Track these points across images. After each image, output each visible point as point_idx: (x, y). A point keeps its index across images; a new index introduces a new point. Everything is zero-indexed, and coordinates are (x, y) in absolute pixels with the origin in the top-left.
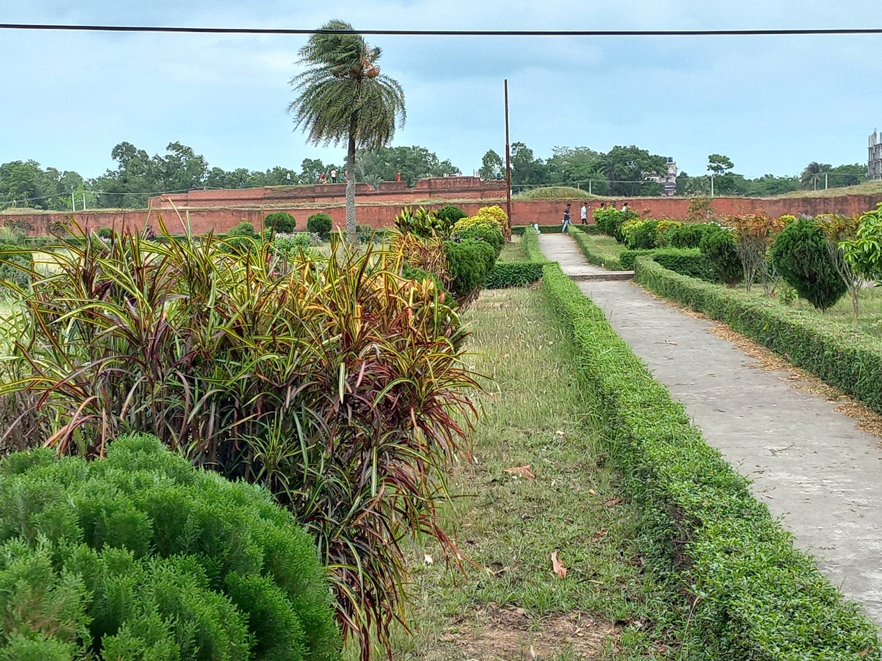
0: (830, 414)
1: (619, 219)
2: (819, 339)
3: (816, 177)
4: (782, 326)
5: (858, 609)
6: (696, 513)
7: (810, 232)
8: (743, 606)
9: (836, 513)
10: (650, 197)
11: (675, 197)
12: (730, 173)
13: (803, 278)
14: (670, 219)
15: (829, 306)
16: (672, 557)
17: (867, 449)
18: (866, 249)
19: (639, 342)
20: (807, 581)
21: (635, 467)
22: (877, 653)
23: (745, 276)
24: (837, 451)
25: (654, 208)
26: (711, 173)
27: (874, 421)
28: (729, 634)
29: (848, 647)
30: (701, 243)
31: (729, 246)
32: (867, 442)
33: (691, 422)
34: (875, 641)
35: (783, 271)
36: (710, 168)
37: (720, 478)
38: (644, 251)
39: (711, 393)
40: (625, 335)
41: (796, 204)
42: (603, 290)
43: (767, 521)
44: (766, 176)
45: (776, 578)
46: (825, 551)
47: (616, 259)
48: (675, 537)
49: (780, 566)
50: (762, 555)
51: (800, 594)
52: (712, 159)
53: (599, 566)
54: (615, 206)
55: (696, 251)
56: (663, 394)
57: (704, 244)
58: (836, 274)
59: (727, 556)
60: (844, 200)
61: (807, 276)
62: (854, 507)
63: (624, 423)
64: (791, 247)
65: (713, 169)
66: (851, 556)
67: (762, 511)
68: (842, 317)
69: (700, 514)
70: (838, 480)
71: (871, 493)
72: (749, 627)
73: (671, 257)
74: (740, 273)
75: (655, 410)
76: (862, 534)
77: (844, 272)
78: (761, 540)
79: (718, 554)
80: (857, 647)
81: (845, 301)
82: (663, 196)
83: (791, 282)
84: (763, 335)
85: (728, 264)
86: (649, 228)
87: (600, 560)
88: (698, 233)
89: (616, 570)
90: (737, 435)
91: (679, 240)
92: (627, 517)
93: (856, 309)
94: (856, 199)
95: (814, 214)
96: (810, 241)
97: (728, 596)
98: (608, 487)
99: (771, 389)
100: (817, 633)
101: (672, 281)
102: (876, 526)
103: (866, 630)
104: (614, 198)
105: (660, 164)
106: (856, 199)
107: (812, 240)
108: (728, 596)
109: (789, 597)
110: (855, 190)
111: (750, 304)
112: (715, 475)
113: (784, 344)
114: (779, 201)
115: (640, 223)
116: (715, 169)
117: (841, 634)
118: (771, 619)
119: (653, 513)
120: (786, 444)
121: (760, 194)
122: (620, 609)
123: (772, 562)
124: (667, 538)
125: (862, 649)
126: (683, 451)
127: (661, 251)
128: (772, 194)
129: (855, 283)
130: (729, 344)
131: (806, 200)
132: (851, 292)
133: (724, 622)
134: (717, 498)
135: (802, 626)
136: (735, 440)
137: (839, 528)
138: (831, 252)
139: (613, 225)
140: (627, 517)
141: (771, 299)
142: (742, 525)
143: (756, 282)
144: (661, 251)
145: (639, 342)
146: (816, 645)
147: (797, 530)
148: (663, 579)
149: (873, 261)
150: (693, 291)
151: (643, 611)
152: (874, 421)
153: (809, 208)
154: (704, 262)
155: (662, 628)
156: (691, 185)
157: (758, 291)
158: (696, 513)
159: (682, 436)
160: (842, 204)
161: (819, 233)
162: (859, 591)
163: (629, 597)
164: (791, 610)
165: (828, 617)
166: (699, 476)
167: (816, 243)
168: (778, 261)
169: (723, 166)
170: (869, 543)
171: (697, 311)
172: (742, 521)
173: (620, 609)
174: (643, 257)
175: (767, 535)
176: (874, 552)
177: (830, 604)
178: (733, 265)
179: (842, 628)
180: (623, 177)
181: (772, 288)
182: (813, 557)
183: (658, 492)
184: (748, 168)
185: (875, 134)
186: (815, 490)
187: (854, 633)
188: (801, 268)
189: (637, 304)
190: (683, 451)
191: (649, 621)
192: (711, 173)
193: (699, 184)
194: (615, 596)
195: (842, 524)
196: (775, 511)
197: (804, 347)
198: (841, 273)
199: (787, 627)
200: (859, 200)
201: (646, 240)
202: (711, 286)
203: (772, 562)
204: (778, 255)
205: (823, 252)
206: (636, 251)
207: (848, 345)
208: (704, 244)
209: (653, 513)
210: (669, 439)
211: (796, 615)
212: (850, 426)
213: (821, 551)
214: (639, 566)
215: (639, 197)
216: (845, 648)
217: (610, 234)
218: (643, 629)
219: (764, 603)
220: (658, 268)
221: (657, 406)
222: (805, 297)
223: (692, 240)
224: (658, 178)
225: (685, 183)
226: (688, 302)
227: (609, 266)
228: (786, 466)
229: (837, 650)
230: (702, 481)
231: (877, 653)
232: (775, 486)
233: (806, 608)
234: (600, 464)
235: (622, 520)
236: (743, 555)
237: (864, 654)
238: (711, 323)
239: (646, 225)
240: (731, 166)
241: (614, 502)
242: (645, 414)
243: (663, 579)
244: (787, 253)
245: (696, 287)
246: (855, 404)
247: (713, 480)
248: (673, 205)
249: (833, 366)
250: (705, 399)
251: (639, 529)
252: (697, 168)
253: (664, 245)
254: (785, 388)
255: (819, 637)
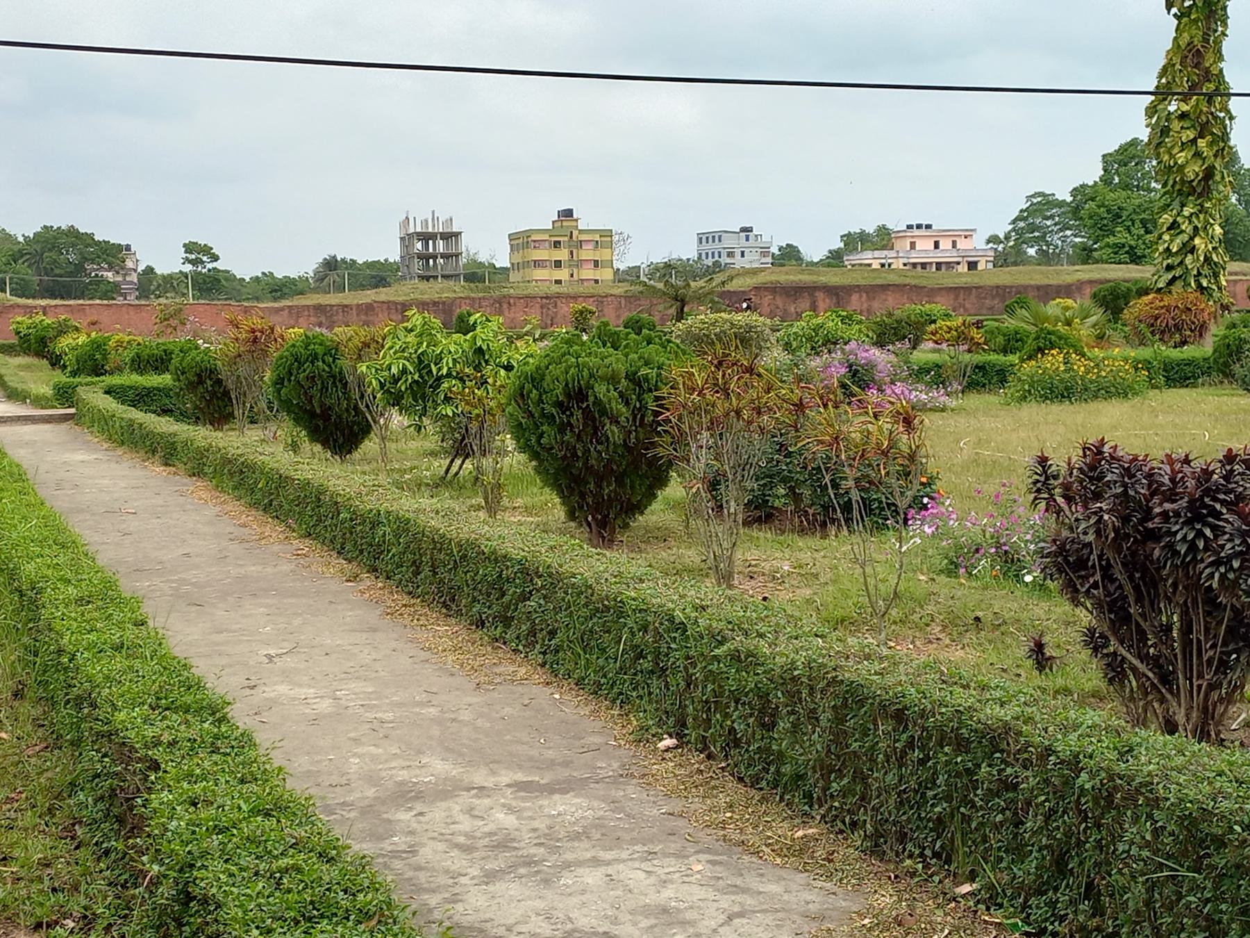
0: (348, 601)
1: (51, 334)
2: (332, 497)
3: (333, 277)
4: (283, 481)
5: (368, 863)
6: (150, 753)
7: (320, 350)
8: (212, 878)
9: (352, 735)
10: (98, 302)
11: (137, 302)
12: (214, 269)
13: (313, 414)
14: (129, 330)
15: (350, 452)
16: (120, 820)
17: (393, 644)
18: (394, 370)
19: (80, 511)
20: (301, 833)
21: (67, 694)
22: (391, 921)
23: (236, 412)
24: (356, 650)
25: (105, 317)
26: (188, 268)
27: (405, 606)
28: (192, 920)
29: (352, 917)
30: (171, 368)
31: (212, 372)
32: (395, 635)
33: (151, 623)
34: (389, 904)
35: (287, 406)
36: (187, 260)
37: (188, 699)
38: (89, 379)
39: (184, 580)
40: (59, 501)
41: (306, 313)
42: (27, 438)
43: (253, 754)
44: (263, 273)
45: (259, 832)
46: (336, 790)
47: (46, 390)
48: (122, 790)
49: (267, 815)
50: (241, 802)
51: (292, 851)
52: (190, 248)
53: (11, 846)
54: (43, 313)
55: (166, 379)
56: (109, 584)
57: (177, 368)
58: (356, 408)
59: (192, 809)
60: (369, 308)
61: (318, 411)
62: (376, 725)
63: (50, 630)
64: (295, 372)
65: (190, 262)
66: (371, 793)
67: (247, 741)
68: (367, 468)
69: (157, 754)
70: (357, 690)
71: (400, 705)
72: (219, 906)
73: (131, 387)
74: (229, 409)
75: (98, 609)
76: (386, 761)
77: (367, 406)
78: (242, 781)
79: (179, 808)
80: (365, 915)
81: (370, 446)
82: (120, 300)
83: (297, 421)
84: (259, 496)
85: (211, 397)
86: (98, 346)
87: (15, 835)
88: (168, 353)
89: (37, 848)
90: (222, 637)
91: (142, 364)
92: (56, 768)
93: (384, 453)
94: (385, 306)
95: (330, 328)
96: (320, 363)
97: (192, 866)
98: (30, 727)
99: (269, 570)
100: (312, 903)
101: (131, 423)
102: (403, 748)
103: (377, 890)
104: (43, 302)
105: (114, 254)
106: (385, 306)
107: (324, 362)
108: (192, 866)
109: (276, 857)
110: (383, 294)
111: (239, 452)
112: (183, 696)
113: (286, 507)
114: (282, 309)
115: (82, 339)
116: (194, 262)
117: (344, 901)
118: (249, 891)
119: (91, 759)
120: (287, 646)
121: (257, 299)
122: (41, 904)
123: (255, 812)
124: (113, 793)
125: (370, 918)
126: (137, 664)
127: (116, 380)
128: (275, 299)
129: (382, 421)
130: (211, 511)
131: (319, 309)
132: (378, 433)
133: (187, 904)
134: (183, 727)
135: (290, 896)
136: (218, 645)
137: (355, 755)
138: (350, 379)
139: (43, 341)
140: (56, 768)
141: (272, 445)
142: (216, 763)
143: (252, 422)
144: (116, 380)
145: (80, 511)
146: (310, 919)
147: (301, 763)
148: (107, 852)
149: (403, 388)
150: (161, 435)
151: (76, 904)
152: (405, 606)
153: (323, 319)
154: (178, 395)
155: (106, 923)
156: (159, 285)
157: (253, 434)
158: (150, 753)
159: (137, 643)
160: (366, 314)
161: (333, 351)
162: (380, 838)
163: (56, 885)
164: (278, 875)
165: (326, 878)
166: (158, 698)
167: (329, 366)
168: (279, 391)
169: (205, 259)
170: (394, 772)
171: (166, 465)
172: (215, 757)
173: (41, 904)
174: (87, 388)
175: (252, 773)
176: (402, 783)
177: (331, 860)
178: (218, 398)
179: (345, 891)
180: (57, 271)
181: (274, 429)
182: (311, 798)
183: (98, 726)
184: (241, 262)
185: (407, 218)
186: (325, 706)
187: (361, 897)
188: (310, 402)
189: (80, 456)
190: (137, 664)
191: (85, 917)
192: (188, 268)
193: (171, 283)
194: (35, 887)
195: (359, 750)
196: (262, 738)
197: (313, 510)
198: (362, 407)
199: (271, 899)
200: (389, 308)
201: (93, 364)
202: (186, 427)
203: (255, 812)
204: (279, 382)
205: (339, 379)
206: (77, 380)
207: (370, 504)
208: (177, 368)
209: (91, 759)
210: (118, 648)
211: (285, 881)
212: (372, 615)
213: (331, 789)
214: (73, 838)
215: (81, 302)
216: (347, 919)
217: (39, 354)
218: (76, 930)
219: (241, 870)
220: (109, 404)
221: (100, 603)
222: (317, 441)
223: (159, 363)
224: (110, 274)
225: (151, 282)
226: (154, 452)
227: (39, 401)
228: (287, 676)
229: (337, 924)
230: (162, 705)
231: (391, 921)
232: (272, 704)
233: (299, 870)
234: (17, 695)
235: (49, 774)
236: (215, 805)
237: (374, 922)
238: (187, 480)
239: (93, 342)
240: (215, 258)
241: (37, 748)
242: (83, 615)
243: (107, 852)
244: (290, 380)
245: (165, 429)
246: (380, 585)
247: (178, 703)
248: (132, 313)
249: (351, 533)
250: (176, 589)
251: (72, 784)
252: (170, 263)
253: (119, 370)
254: (285, 567)
255: (314, 908)
